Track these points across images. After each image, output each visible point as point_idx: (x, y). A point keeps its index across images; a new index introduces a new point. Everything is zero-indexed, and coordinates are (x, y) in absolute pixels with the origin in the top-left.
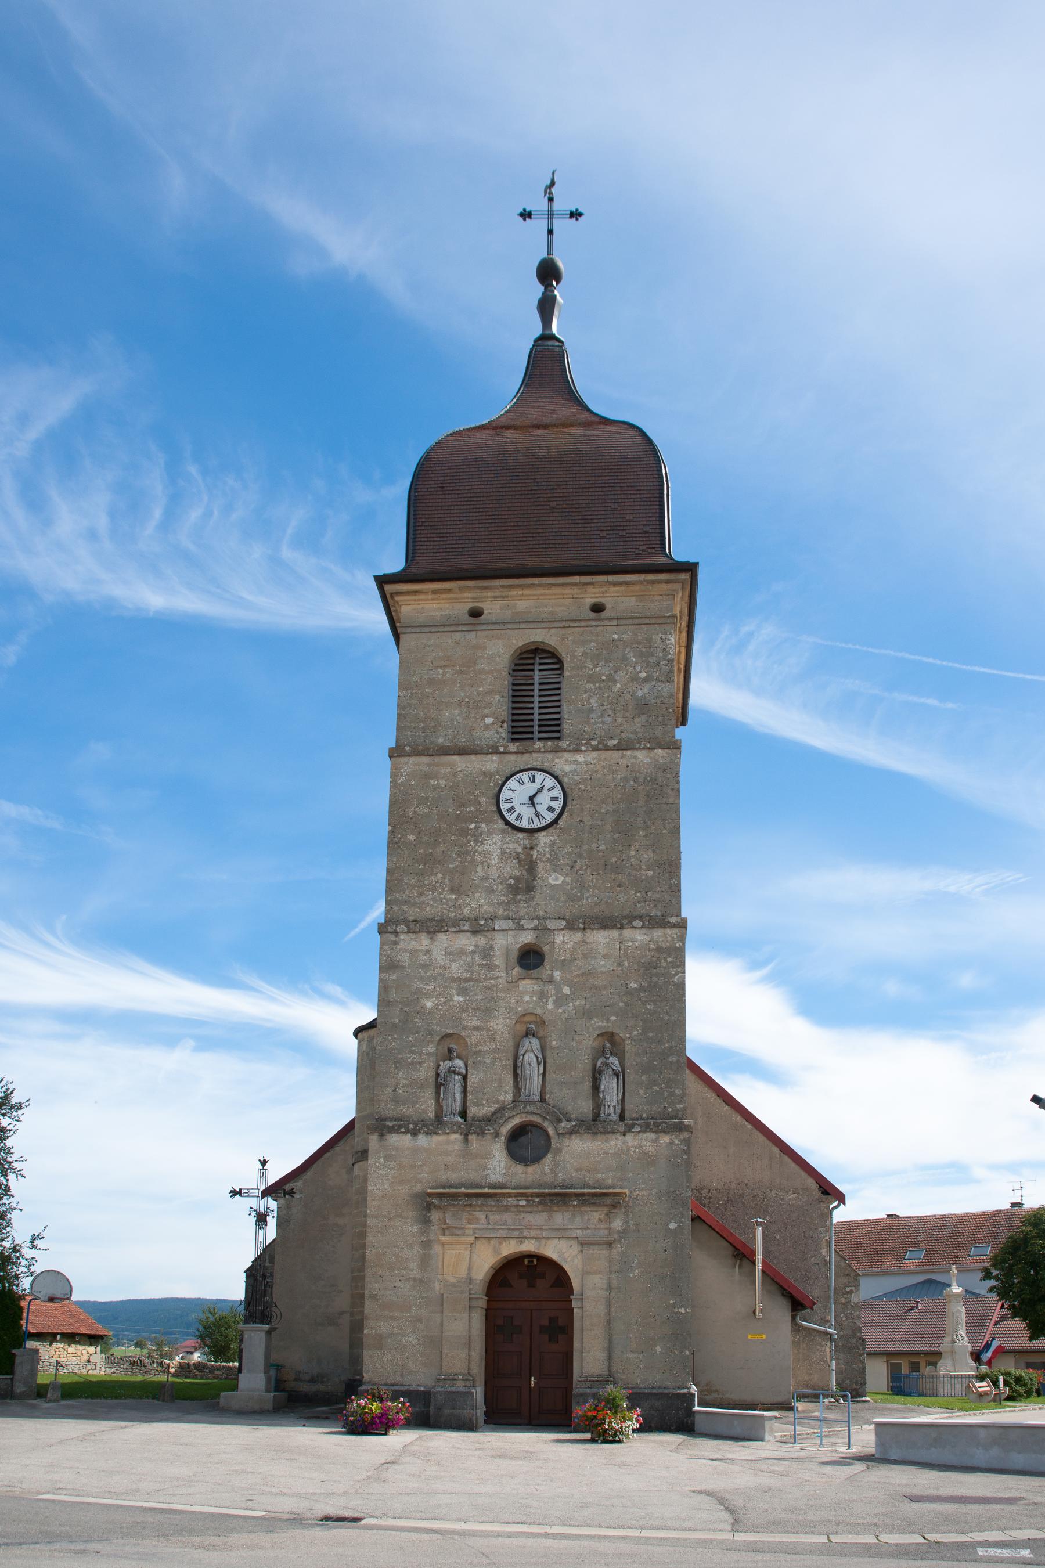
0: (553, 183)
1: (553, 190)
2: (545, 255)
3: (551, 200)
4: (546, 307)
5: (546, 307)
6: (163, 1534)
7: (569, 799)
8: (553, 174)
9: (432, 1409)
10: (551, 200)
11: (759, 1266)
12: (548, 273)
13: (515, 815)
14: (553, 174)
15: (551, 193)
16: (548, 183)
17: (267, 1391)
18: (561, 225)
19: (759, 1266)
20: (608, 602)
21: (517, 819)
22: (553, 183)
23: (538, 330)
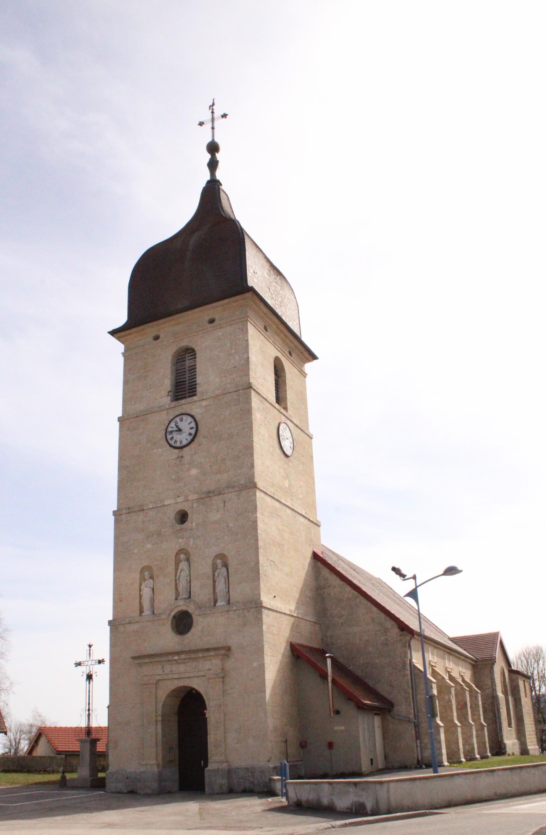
0: (213, 104)
1: (214, 107)
2: (210, 140)
3: (213, 112)
4: (213, 165)
5: (213, 165)
6: (372, 772)
7: (165, 439)
8: (213, 100)
9: (366, 723)
10: (213, 112)
11: (330, 679)
12: (213, 148)
13: (174, 441)
14: (213, 100)
15: (213, 109)
16: (211, 104)
17: (90, 776)
18: (219, 123)
19: (330, 679)
20: (217, 317)
21: (174, 443)
22: (213, 104)
23: (208, 178)
